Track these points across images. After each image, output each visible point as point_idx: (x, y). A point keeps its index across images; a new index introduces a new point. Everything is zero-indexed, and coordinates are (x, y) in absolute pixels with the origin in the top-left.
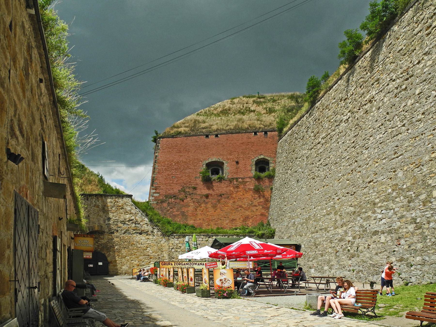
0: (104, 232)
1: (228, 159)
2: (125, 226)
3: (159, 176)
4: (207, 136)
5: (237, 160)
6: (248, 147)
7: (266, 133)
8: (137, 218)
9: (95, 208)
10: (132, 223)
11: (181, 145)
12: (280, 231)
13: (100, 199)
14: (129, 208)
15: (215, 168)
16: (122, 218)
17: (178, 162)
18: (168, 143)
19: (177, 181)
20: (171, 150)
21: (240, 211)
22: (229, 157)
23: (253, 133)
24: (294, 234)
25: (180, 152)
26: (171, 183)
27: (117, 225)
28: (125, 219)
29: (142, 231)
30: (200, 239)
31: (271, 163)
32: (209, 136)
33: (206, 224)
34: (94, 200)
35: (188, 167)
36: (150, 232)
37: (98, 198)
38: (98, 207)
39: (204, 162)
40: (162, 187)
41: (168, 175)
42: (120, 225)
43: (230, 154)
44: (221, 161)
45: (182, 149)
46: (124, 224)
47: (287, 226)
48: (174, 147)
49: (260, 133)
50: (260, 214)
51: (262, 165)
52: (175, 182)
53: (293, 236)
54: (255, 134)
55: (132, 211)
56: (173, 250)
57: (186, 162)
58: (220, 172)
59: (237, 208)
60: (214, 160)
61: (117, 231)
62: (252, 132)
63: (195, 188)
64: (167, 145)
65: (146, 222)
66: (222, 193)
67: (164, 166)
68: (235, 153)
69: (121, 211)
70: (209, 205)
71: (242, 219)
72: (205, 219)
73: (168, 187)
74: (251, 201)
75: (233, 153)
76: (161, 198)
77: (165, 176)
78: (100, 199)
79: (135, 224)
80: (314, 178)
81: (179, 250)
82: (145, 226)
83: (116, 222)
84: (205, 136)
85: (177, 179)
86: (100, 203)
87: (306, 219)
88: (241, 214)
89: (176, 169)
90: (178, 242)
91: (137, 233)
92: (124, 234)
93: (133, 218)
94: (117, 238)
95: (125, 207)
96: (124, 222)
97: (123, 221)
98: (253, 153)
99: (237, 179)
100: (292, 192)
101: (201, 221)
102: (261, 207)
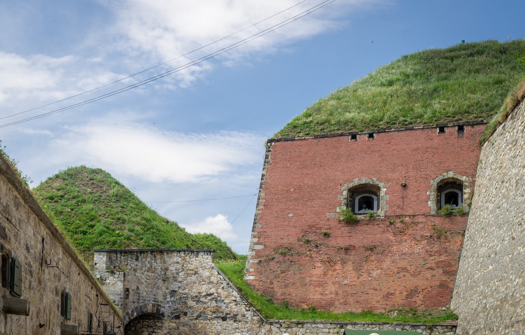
0: (163, 315)
2: (200, 305)
4: (354, 137)
5: (403, 182)
7: (461, 128)
8: (220, 291)
9: (150, 274)
11: (307, 153)
12: (466, 319)
13: (158, 257)
15: (363, 197)
16: (194, 290)
21: (403, 278)
22: (390, 175)
23: (438, 130)
24: (482, 326)
28: (200, 293)
30: (324, 330)
31: (466, 186)
32: (358, 136)
33: (342, 301)
34: (149, 259)
36: (239, 317)
37: (155, 257)
39: (346, 185)
44: (377, 183)
47: (476, 309)
49: (450, 129)
50: (438, 283)
51: (451, 193)
52: (291, 224)
53: (481, 330)
54: (442, 130)
55: (212, 279)
57: (314, 186)
58: (375, 203)
59: (398, 273)
61: (185, 314)
62: (436, 128)
65: (233, 298)
68: (401, 168)
69: (194, 278)
70: (349, 267)
71: (405, 293)
74: (425, 260)
76: (267, 253)
77: (277, 212)
80: (521, 224)
82: (233, 305)
83: (184, 298)
84: (350, 137)
86: (158, 265)
87: (501, 300)
88: (404, 284)
89: (296, 199)
92: (196, 319)
93: (213, 290)
94: (183, 326)
95: (201, 271)
97: (196, 297)
98: (433, 169)
100: (490, 246)
102: (441, 271)
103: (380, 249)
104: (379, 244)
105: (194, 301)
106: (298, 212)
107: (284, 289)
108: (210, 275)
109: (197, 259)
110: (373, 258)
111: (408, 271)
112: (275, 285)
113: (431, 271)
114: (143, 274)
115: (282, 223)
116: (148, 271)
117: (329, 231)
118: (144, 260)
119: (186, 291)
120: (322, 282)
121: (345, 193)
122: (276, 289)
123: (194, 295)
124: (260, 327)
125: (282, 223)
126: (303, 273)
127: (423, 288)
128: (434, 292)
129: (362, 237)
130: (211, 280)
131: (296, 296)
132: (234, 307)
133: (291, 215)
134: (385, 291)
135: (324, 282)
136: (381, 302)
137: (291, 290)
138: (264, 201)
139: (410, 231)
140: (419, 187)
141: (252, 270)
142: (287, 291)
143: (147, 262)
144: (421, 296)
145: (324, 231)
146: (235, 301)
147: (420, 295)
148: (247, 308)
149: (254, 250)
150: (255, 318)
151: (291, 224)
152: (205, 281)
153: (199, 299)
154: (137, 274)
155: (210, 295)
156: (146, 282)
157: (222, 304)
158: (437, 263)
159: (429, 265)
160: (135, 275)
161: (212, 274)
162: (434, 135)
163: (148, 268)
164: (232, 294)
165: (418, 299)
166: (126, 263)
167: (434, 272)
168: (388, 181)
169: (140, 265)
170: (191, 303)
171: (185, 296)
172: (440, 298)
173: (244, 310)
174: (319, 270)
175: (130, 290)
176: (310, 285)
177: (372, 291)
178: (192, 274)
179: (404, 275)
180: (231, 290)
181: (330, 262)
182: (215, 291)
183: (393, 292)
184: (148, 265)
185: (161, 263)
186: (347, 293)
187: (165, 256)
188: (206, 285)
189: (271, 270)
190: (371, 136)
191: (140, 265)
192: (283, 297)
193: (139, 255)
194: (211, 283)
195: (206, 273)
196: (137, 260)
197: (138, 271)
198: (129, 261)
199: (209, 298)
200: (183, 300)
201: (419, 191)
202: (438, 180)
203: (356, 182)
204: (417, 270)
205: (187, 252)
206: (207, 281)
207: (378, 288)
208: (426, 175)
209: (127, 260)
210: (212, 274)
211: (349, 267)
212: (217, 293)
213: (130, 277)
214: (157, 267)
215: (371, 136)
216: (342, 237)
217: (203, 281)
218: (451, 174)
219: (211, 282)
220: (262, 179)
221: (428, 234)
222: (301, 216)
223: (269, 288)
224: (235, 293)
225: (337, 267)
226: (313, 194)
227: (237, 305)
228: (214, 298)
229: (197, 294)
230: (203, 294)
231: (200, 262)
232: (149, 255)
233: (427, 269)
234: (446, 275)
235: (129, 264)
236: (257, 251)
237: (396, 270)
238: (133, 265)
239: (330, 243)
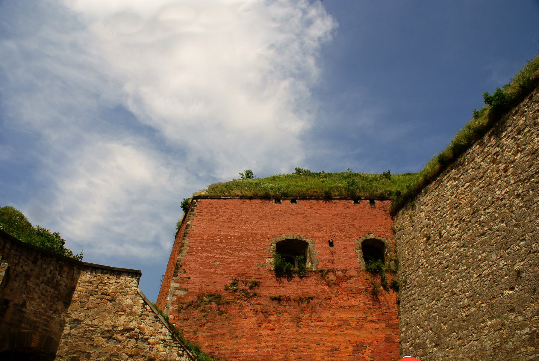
1: (315, 238)
2: (111, 344)
3: (191, 258)
6: (346, 220)
8: (143, 325)
10: (130, 337)
11: (233, 210)
13: (66, 269)
14: (130, 301)
16: (107, 322)
17: (226, 238)
18: (210, 206)
19: (224, 269)
20: (214, 218)
21: (346, 331)
22: (316, 234)
25: (231, 221)
26: (212, 273)
27: (91, 339)
28: (114, 326)
35: (243, 246)
37: (61, 267)
38: (56, 286)
40: (193, 278)
41: (207, 258)
42: (99, 339)
43: (319, 230)
44: (304, 239)
45: (234, 218)
46: (110, 338)
48: (222, 213)
50: (382, 337)
52: (219, 271)
57: (241, 238)
59: (340, 326)
60: (290, 237)
63: (256, 284)
64: (208, 210)
65: (162, 337)
67: (201, 243)
68: (325, 228)
70: (286, 318)
71: (351, 348)
72: (277, 346)
73: (206, 280)
75: (322, 229)
77: (202, 259)
78: (66, 269)
79: (137, 339)
82: (160, 346)
85: (222, 266)
88: (348, 338)
89: (222, 249)
96: (109, 335)
97: (109, 331)
99: (333, 271)
101: (270, 350)
104: (315, 295)
105: (103, 338)
107: (211, 341)
108: (133, 303)
109: (118, 281)
111: (350, 323)
112: (200, 336)
113: (374, 324)
114: (37, 285)
115: (208, 270)
116: (46, 284)
118: (44, 266)
119: (95, 322)
120: (256, 334)
122: (201, 341)
123: (106, 329)
125: (208, 270)
126: (233, 324)
127: (369, 342)
128: (381, 347)
129: (292, 288)
130: (133, 310)
131: (225, 349)
132: (162, 349)
134: (329, 345)
135: (258, 335)
137: (220, 342)
138: (188, 248)
140: (346, 245)
142: (214, 343)
143: (48, 271)
144: (368, 352)
146: (164, 341)
147: (367, 350)
148: (181, 352)
149: (175, 295)
151: (219, 271)
152: (125, 311)
153: (113, 334)
154: (30, 284)
155: (129, 330)
156: (39, 298)
157: (145, 345)
158: (378, 316)
159: (369, 318)
160: (25, 283)
161: (135, 303)
162: (350, 205)
163: (48, 278)
164: (160, 330)
166: (17, 262)
167: (377, 326)
169: (37, 270)
170: (99, 339)
171: (93, 329)
172: (389, 354)
173: (176, 354)
174: (250, 322)
175: (11, 304)
176: (242, 337)
178: (108, 300)
179: (346, 329)
180: (159, 325)
182: (137, 325)
183: (337, 346)
184: (49, 276)
185: (67, 278)
186: (286, 347)
187: (75, 272)
188: (124, 317)
189: (194, 318)
191: (37, 270)
192: (209, 350)
193: (39, 257)
194: (132, 313)
195: (128, 301)
196: (35, 262)
197: (32, 279)
198: (21, 261)
200: (88, 335)
201: (346, 248)
204: (359, 323)
205: (105, 271)
206: (128, 311)
207: (321, 342)
208: (349, 235)
209: (20, 258)
210: (135, 303)
211: (286, 318)
212: (140, 328)
213: (16, 284)
214: (61, 282)
216: (272, 287)
217: (122, 310)
219: (133, 312)
221: (363, 288)
222: (229, 264)
223: (192, 338)
224: (164, 330)
225: (272, 318)
227: (166, 347)
228: (134, 335)
229: (110, 329)
230: (119, 329)
231: (121, 285)
232: (54, 262)
233: (369, 322)
234: (389, 328)
235: (21, 265)
236: (179, 298)
238: (26, 268)
239: (262, 292)
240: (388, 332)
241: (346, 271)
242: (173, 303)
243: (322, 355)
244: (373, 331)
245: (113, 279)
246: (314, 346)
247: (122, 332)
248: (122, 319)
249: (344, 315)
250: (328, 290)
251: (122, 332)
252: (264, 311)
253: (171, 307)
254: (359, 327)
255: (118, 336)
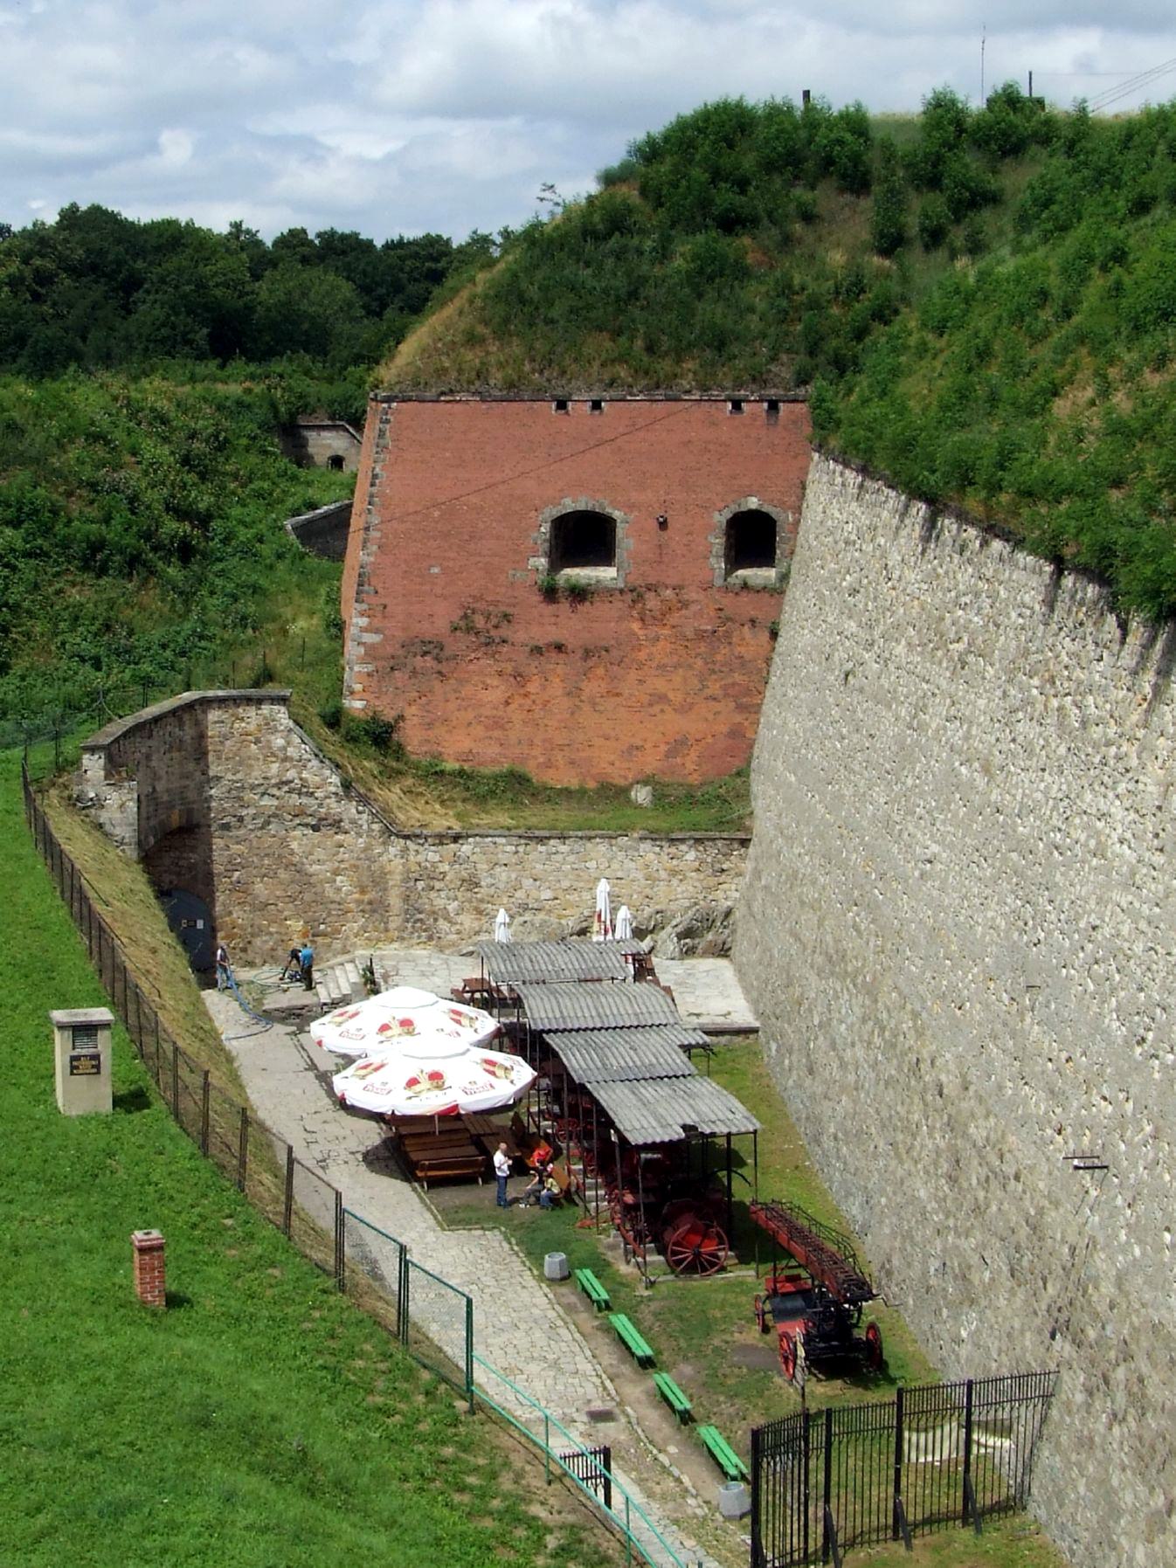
4: (562, 405)
16: (256, 773)
21: (660, 716)
22: (635, 496)
23: (730, 405)
27: (240, 799)
29: (321, 819)
32: (570, 404)
36: (345, 825)
44: (609, 510)
50: (725, 729)
55: (291, 751)
56: (420, 885)
59: (651, 705)
60: (581, 507)
61: (241, 819)
66: (604, 643)
71: (664, 748)
81: (438, 885)
84: (554, 405)
88: (661, 729)
90: (437, 858)
91: (306, 825)
93: (291, 774)
103: (615, 653)
106: (451, 564)
110: (600, 671)
117: (510, 611)
119: (239, 776)
121: (545, 528)
124: (384, 843)
132: (334, 805)
133: (436, 570)
136: (617, 764)
139: (674, 618)
141: (358, 687)
144: (693, 755)
145: (503, 608)
150: (375, 827)
159: (708, 692)
165: (690, 761)
168: (631, 507)
177: (601, 741)
181: (519, 677)
183: (640, 743)
190: (596, 405)
194: (286, 759)
199: (286, 788)
202: (728, 514)
203: (569, 505)
206: (281, 755)
207: (613, 734)
215: (596, 405)
218: (753, 503)
220: (372, 485)
226: (481, 526)
237: (646, 699)
240: (738, 718)
241: (681, 587)
242: (363, 661)
243: (612, 757)
244: (710, 717)
245: (251, 711)
246: (598, 742)
247: (279, 786)
248: (275, 768)
249: (660, 685)
250: (640, 632)
251: (279, 786)
252: (517, 675)
253: (356, 668)
254: (685, 709)
255: (275, 791)
